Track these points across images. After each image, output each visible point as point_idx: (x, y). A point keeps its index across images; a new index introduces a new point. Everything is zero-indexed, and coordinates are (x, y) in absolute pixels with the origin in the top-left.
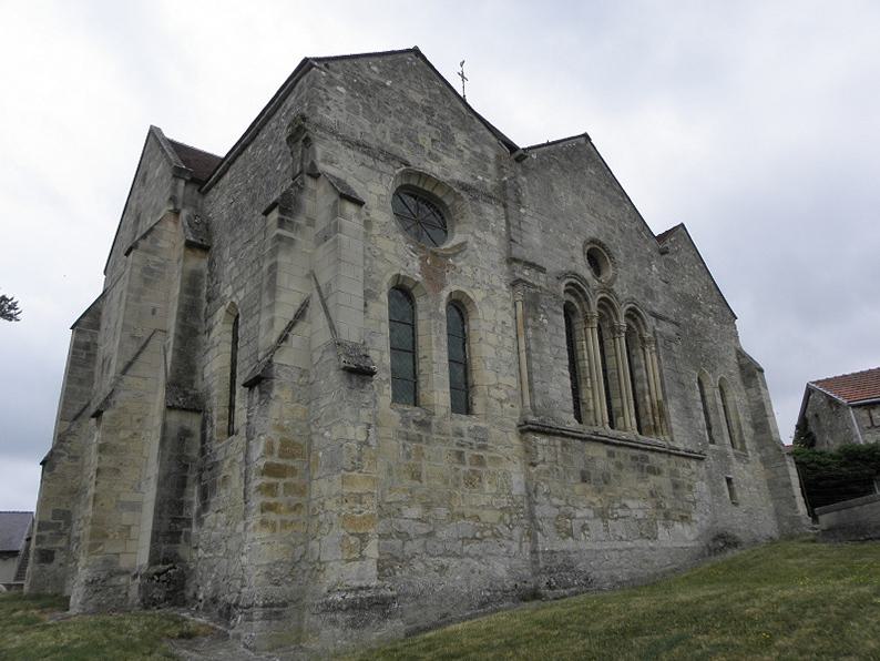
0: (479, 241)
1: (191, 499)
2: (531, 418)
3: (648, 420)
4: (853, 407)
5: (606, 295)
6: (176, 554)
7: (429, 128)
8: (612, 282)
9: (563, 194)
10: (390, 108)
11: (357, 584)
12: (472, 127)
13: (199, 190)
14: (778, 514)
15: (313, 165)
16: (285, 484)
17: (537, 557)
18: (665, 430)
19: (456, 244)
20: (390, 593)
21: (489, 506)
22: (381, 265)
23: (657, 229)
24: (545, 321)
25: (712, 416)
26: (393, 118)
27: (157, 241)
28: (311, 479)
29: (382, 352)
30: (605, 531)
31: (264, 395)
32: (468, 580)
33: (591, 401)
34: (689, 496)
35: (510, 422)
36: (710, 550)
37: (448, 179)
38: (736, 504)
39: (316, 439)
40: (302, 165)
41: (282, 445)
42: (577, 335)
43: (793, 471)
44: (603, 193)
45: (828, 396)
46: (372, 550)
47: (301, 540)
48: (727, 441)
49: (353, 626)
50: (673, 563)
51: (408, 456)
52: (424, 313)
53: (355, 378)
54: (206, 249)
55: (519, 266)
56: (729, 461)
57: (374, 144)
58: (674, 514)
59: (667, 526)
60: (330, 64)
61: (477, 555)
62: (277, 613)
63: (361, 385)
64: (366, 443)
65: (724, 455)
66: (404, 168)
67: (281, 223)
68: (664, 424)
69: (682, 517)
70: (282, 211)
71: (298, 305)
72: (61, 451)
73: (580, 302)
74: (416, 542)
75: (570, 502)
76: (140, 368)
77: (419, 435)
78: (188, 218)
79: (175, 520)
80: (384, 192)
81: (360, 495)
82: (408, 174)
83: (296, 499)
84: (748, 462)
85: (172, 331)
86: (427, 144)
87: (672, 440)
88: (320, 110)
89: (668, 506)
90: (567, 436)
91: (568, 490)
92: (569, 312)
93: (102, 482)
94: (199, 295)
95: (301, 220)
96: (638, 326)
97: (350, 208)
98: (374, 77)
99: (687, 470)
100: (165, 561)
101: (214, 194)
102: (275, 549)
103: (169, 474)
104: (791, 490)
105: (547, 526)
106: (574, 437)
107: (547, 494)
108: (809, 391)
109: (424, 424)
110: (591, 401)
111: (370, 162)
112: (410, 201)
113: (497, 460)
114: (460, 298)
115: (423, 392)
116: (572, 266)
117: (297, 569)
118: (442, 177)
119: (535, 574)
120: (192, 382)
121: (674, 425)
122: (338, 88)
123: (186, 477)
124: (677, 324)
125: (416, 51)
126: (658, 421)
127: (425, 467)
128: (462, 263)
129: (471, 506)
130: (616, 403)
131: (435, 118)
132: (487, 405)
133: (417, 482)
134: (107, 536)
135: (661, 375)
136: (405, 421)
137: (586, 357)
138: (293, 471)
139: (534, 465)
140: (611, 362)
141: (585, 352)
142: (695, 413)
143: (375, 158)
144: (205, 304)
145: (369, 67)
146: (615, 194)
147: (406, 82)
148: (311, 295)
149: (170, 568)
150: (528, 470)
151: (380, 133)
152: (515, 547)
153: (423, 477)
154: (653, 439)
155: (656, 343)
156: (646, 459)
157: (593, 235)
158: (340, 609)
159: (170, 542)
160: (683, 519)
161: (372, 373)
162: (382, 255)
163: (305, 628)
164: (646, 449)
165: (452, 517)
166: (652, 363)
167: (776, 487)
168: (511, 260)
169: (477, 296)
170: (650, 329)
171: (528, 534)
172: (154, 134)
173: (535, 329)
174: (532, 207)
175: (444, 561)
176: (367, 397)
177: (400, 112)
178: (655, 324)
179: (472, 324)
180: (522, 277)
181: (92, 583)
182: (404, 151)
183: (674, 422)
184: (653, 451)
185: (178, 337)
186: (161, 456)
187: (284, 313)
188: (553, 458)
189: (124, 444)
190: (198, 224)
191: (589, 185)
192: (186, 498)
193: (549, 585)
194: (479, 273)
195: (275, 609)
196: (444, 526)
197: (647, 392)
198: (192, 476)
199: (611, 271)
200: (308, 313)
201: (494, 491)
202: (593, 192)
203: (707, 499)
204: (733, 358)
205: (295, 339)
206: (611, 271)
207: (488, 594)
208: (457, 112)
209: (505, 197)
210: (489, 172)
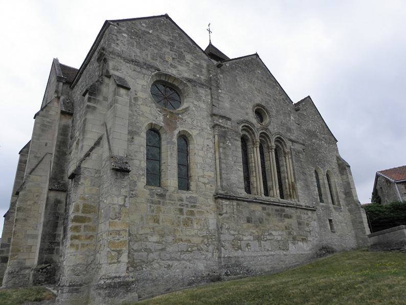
0: (195, 106)
1: (60, 233)
2: (221, 192)
3: (286, 192)
4: (397, 183)
5: (264, 131)
6: (52, 259)
7: (171, 53)
8: (268, 125)
9: (242, 83)
10: (151, 43)
11: (114, 275)
12: (195, 51)
13: (70, 87)
14: (357, 237)
15: (107, 71)
16: (84, 226)
17: (221, 260)
18: (295, 196)
19: (184, 108)
20: (131, 280)
21: (196, 235)
22: (142, 119)
23: (295, 100)
24: (230, 144)
25: (322, 190)
26: (152, 48)
27: (49, 111)
28: (99, 223)
29: (140, 161)
30: (259, 246)
31: (76, 183)
32: (183, 272)
33: (255, 183)
34: (307, 229)
35: (210, 194)
36: (318, 255)
37: (180, 76)
38: (334, 232)
39: (101, 204)
40: (102, 71)
41: (83, 207)
42: (249, 151)
43: (364, 216)
44: (265, 82)
45: (385, 178)
46: (124, 258)
47: (92, 253)
48: (330, 201)
49: (109, 296)
50: (297, 262)
51: (153, 211)
52: (165, 141)
53: (119, 174)
54: (71, 114)
55: (216, 118)
56: (331, 211)
57: (141, 60)
58: (298, 238)
59: (294, 244)
60: (120, 23)
61: (188, 259)
62: (77, 289)
63: (122, 177)
64: (124, 205)
65: (328, 208)
66: (157, 72)
67: (89, 100)
68: (294, 193)
69: (303, 239)
70: (91, 94)
71: (97, 139)
72: (13, 211)
73: (250, 135)
74: (155, 253)
75: (240, 233)
76: (39, 171)
77: (159, 201)
78: (64, 101)
79: (51, 243)
80: (145, 84)
81: (119, 231)
82: (160, 74)
83: (91, 233)
84: (341, 211)
85: (54, 154)
86: (170, 60)
87: (299, 201)
88: (113, 45)
89: (295, 234)
90: (240, 200)
91: (239, 227)
92: (244, 140)
93: (18, 225)
94: (67, 136)
95: (100, 98)
96: (282, 146)
97: (123, 91)
98: (143, 29)
99: (305, 216)
100: (46, 263)
101: (76, 89)
102: (78, 258)
103: (49, 221)
104: (363, 225)
105: (227, 245)
106: (244, 201)
107: (228, 229)
108: (377, 176)
109: (162, 196)
110: (255, 183)
111: (138, 69)
112: (161, 87)
113: (201, 213)
114: (185, 134)
115: (163, 180)
116: (246, 117)
117: (89, 267)
118: (177, 76)
119: (220, 268)
120: (62, 177)
121: (300, 194)
122: (123, 34)
123: (58, 222)
124: (304, 145)
125: (166, 16)
126: (292, 192)
127: (162, 217)
128: (186, 117)
129: (187, 235)
130: (269, 184)
131: (175, 48)
132: (197, 186)
133: (157, 224)
134: (19, 251)
135: (293, 170)
136: (152, 195)
137: (253, 162)
138: (89, 220)
139: (221, 215)
140: (267, 163)
141: (253, 159)
142: (312, 188)
143: (141, 67)
144: (70, 140)
145: (141, 24)
146: (271, 82)
147: (160, 31)
148: (104, 134)
149: (49, 266)
150: (218, 217)
151: (146, 56)
152: (210, 255)
153: (160, 221)
154: (289, 201)
155: (291, 154)
156: (284, 211)
157: (258, 102)
158: (102, 288)
159: (49, 253)
160: (303, 240)
161: (128, 171)
162: (143, 114)
163: (90, 297)
164: (284, 206)
165: (175, 241)
166: (289, 165)
167: (356, 223)
168: (213, 115)
169: (194, 133)
170: (288, 147)
171: (217, 249)
172: (55, 63)
173: (224, 148)
174: (225, 89)
175: (170, 263)
176: (126, 182)
177: (156, 45)
178: (291, 144)
179: (191, 146)
180: (218, 123)
181: (12, 272)
182: (158, 64)
183: (300, 192)
184: (287, 207)
185: (56, 156)
186: (46, 212)
187: (89, 142)
188: (232, 211)
189: (29, 207)
190: (68, 103)
191: (257, 78)
192: (58, 233)
193: (227, 274)
194: (195, 122)
195: (75, 287)
196: (170, 245)
197: (286, 178)
198: (60, 222)
199: (268, 120)
200: (101, 143)
201: (199, 228)
202: (259, 81)
203: (317, 230)
204: (335, 161)
205: (94, 155)
206: (268, 120)
207: (193, 278)
208: (187, 45)
209: (211, 84)
210: (203, 73)
